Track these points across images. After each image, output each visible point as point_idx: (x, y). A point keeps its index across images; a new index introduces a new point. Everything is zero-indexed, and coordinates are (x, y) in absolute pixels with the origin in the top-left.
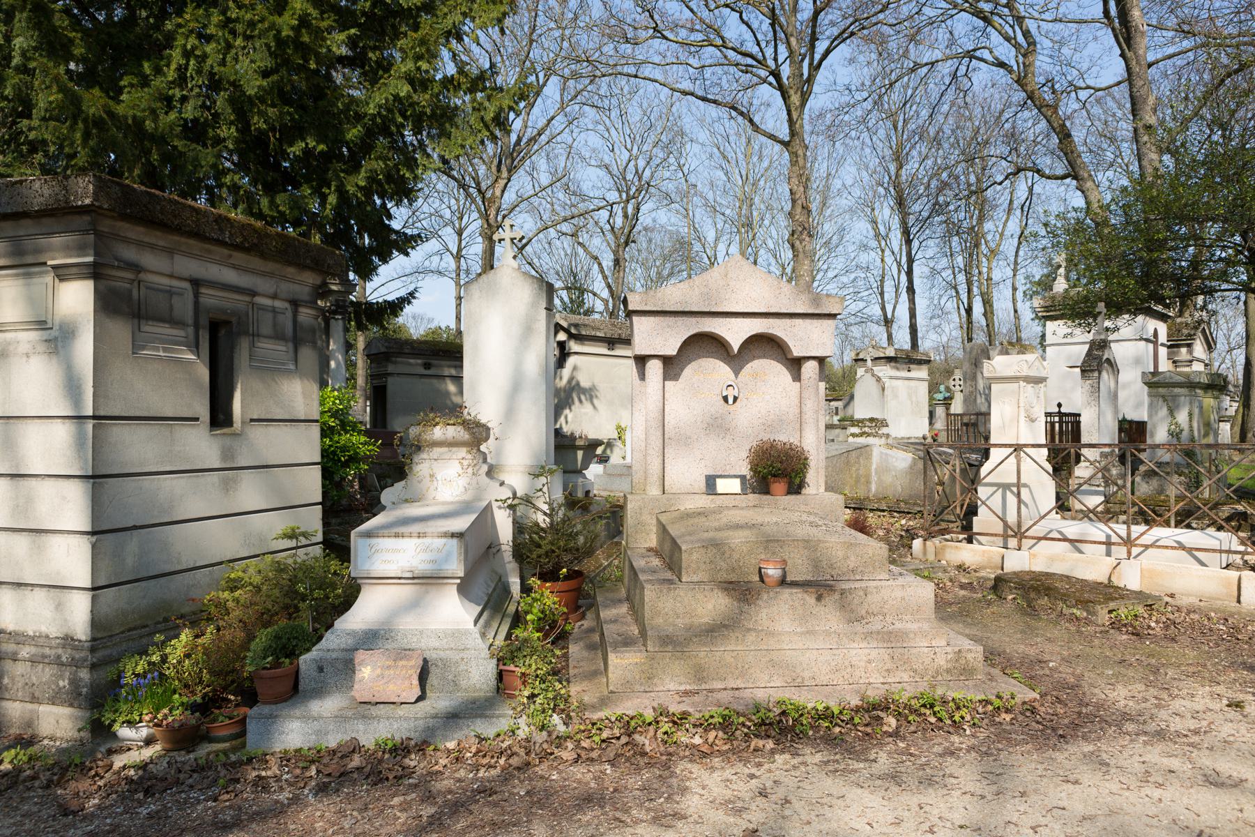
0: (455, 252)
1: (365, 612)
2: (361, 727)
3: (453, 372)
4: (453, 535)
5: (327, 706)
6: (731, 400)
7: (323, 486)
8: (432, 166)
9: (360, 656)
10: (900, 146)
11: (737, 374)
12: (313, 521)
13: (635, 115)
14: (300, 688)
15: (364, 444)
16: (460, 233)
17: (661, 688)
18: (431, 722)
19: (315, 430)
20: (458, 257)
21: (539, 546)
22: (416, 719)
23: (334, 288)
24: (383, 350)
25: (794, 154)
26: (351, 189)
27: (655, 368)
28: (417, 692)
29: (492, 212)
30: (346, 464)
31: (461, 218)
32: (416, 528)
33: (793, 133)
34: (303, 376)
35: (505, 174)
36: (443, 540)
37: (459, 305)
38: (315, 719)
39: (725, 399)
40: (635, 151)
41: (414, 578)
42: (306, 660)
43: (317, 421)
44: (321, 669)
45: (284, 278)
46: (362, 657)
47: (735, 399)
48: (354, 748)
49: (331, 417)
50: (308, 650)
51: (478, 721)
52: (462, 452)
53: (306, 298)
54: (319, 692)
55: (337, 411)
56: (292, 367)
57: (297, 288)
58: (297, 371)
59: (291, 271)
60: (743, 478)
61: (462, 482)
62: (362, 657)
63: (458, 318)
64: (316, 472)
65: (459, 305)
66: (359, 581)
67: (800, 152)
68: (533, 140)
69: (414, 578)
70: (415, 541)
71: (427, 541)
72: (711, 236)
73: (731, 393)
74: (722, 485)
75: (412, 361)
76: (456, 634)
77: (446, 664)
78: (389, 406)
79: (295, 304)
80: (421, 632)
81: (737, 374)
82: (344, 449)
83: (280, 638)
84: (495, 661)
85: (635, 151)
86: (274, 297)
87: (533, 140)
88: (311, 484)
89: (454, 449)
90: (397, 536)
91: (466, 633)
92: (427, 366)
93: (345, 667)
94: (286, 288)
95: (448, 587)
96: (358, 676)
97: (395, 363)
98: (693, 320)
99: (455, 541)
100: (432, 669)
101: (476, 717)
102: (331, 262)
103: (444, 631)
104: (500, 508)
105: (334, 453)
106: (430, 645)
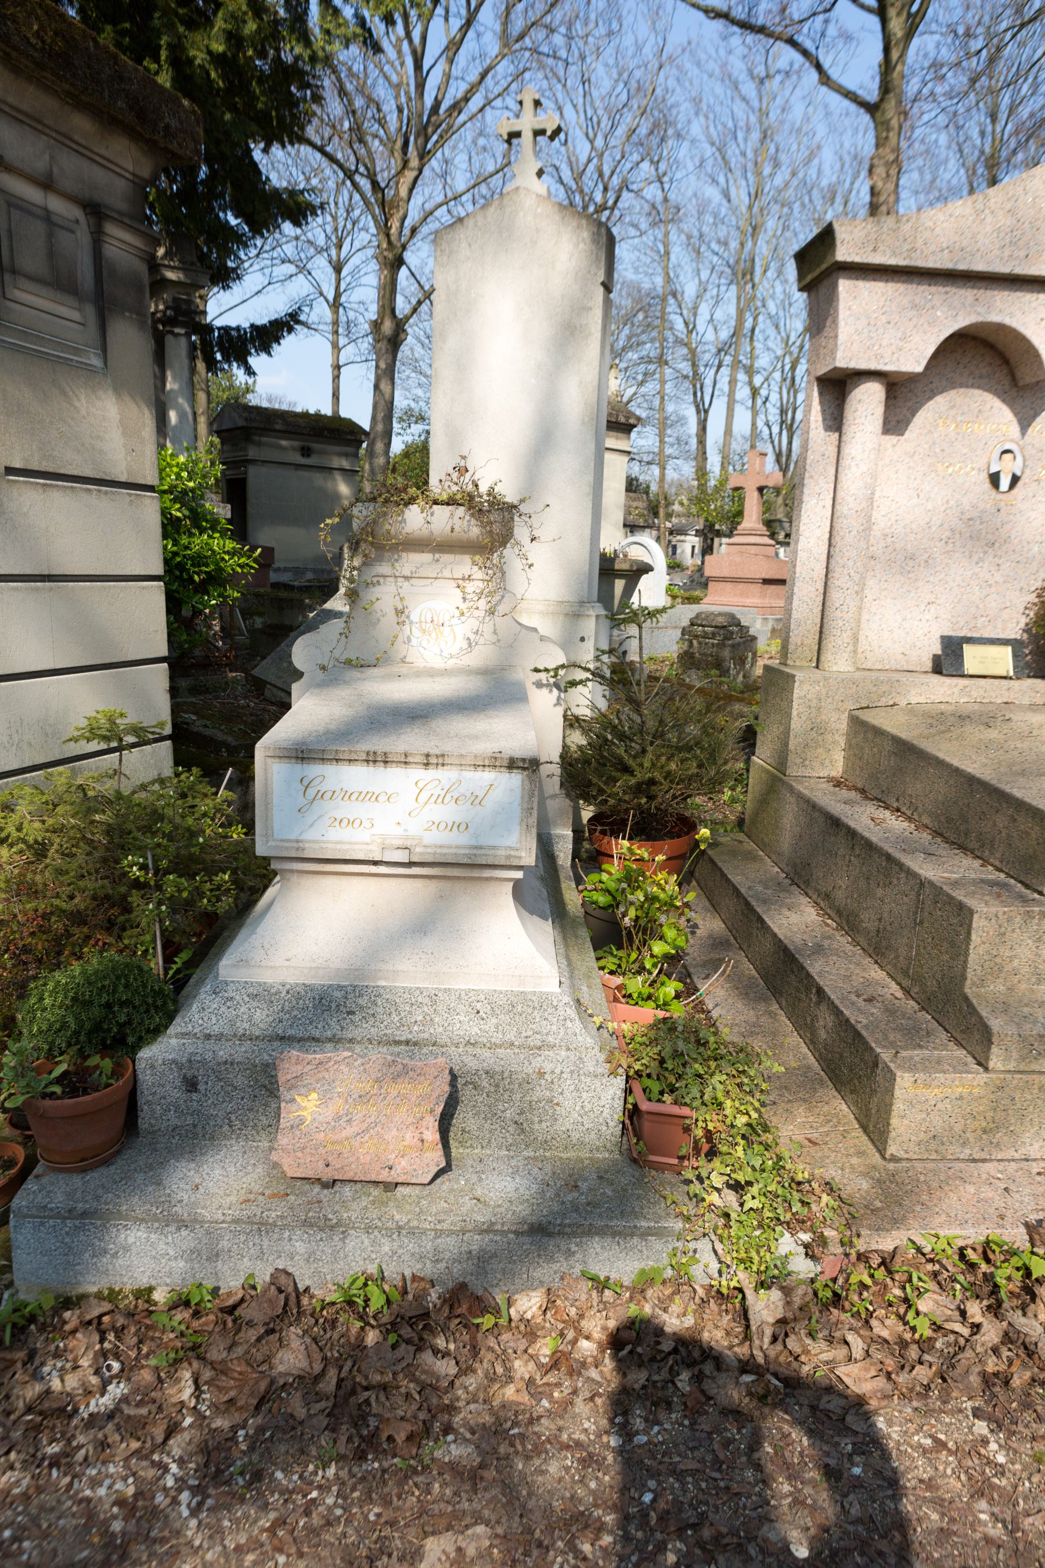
0: (331, 297)
1: (299, 937)
2: (300, 1247)
3: (345, 464)
4: (512, 765)
5: (219, 1182)
6: (1005, 482)
7: (169, 624)
8: (341, 31)
9: (293, 1064)
10: (998, 144)
11: (1025, 424)
12: (151, 696)
13: (603, 79)
14: (143, 1124)
15: (233, 553)
16: (338, 268)
17: (1011, 1153)
18: (476, 1243)
19: (149, 511)
20: (336, 305)
21: (627, 770)
22: (439, 1233)
23: (171, 275)
24: (241, 423)
25: (882, 126)
26: (200, 57)
27: (867, 402)
28: (435, 1158)
29: (395, 224)
30: (202, 588)
31: (339, 246)
32: (411, 740)
33: (886, 88)
34: (119, 389)
35: (414, 163)
36: (488, 776)
37: (336, 378)
38: (182, 1224)
39: (994, 479)
40: (599, 142)
41: (411, 864)
42: (156, 1056)
43: (151, 488)
44: (191, 1085)
45: (64, 139)
46: (296, 1070)
47: (1015, 480)
48: (287, 1301)
49: (174, 501)
50: (157, 1032)
51: (596, 1244)
52: (464, 565)
53: (122, 206)
54: (194, 1138)
55: (184, 492)
56: (96, 362)
57: (98, 175)
58: (106, 371)
59: (81, 124)
60: (1015, 644)
61: (464, 628)
62: (296, 1070)
63: (336, 396)
64: (155, 596)
65: (336, 378)
66: (274, 865)
67: (894, 123)
68: (457, 107)
69: (411, 864)
70: (418, 774)
71: (445, 776)
72: (690, 290)
73: (1007, 468)
74: (973, 658)
75: (284, 443)
76: (521, 1005)
77: (499, 1081)
78: (250, 509)
79: (96, 212)
80: (434, 998)
81: (1025, 424)
82: (199, 560)
83: (88, 1004)
84: (620, 1082)
85: (599, 142)
86: (47, 184)
87: (457, 107)
88: (142, 619)
89: (447, 558)
90: (372, 759)
91: (543, 1003)
92: (306, 452)
93: (257, 1089)
94: (71, 168)
95: (493, 887)
96: (288, 1115)
97: (259, 444)
98: (965, 295)
99: (515, 780)
100: (466, 1094)
101: (591, 1232)
102: (174, 123)
103: (490, 998)
104: (539, 685)
105: (181, 566)
106: (463, 1031)
